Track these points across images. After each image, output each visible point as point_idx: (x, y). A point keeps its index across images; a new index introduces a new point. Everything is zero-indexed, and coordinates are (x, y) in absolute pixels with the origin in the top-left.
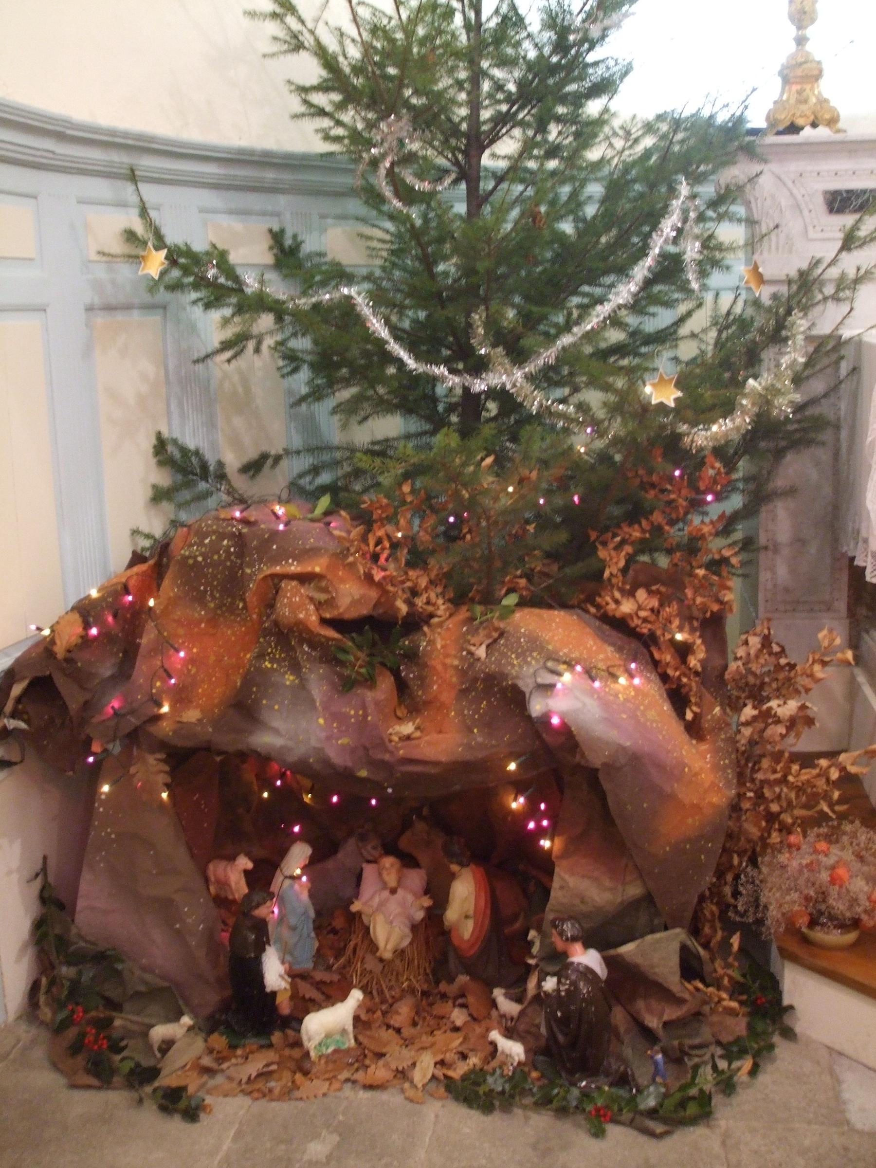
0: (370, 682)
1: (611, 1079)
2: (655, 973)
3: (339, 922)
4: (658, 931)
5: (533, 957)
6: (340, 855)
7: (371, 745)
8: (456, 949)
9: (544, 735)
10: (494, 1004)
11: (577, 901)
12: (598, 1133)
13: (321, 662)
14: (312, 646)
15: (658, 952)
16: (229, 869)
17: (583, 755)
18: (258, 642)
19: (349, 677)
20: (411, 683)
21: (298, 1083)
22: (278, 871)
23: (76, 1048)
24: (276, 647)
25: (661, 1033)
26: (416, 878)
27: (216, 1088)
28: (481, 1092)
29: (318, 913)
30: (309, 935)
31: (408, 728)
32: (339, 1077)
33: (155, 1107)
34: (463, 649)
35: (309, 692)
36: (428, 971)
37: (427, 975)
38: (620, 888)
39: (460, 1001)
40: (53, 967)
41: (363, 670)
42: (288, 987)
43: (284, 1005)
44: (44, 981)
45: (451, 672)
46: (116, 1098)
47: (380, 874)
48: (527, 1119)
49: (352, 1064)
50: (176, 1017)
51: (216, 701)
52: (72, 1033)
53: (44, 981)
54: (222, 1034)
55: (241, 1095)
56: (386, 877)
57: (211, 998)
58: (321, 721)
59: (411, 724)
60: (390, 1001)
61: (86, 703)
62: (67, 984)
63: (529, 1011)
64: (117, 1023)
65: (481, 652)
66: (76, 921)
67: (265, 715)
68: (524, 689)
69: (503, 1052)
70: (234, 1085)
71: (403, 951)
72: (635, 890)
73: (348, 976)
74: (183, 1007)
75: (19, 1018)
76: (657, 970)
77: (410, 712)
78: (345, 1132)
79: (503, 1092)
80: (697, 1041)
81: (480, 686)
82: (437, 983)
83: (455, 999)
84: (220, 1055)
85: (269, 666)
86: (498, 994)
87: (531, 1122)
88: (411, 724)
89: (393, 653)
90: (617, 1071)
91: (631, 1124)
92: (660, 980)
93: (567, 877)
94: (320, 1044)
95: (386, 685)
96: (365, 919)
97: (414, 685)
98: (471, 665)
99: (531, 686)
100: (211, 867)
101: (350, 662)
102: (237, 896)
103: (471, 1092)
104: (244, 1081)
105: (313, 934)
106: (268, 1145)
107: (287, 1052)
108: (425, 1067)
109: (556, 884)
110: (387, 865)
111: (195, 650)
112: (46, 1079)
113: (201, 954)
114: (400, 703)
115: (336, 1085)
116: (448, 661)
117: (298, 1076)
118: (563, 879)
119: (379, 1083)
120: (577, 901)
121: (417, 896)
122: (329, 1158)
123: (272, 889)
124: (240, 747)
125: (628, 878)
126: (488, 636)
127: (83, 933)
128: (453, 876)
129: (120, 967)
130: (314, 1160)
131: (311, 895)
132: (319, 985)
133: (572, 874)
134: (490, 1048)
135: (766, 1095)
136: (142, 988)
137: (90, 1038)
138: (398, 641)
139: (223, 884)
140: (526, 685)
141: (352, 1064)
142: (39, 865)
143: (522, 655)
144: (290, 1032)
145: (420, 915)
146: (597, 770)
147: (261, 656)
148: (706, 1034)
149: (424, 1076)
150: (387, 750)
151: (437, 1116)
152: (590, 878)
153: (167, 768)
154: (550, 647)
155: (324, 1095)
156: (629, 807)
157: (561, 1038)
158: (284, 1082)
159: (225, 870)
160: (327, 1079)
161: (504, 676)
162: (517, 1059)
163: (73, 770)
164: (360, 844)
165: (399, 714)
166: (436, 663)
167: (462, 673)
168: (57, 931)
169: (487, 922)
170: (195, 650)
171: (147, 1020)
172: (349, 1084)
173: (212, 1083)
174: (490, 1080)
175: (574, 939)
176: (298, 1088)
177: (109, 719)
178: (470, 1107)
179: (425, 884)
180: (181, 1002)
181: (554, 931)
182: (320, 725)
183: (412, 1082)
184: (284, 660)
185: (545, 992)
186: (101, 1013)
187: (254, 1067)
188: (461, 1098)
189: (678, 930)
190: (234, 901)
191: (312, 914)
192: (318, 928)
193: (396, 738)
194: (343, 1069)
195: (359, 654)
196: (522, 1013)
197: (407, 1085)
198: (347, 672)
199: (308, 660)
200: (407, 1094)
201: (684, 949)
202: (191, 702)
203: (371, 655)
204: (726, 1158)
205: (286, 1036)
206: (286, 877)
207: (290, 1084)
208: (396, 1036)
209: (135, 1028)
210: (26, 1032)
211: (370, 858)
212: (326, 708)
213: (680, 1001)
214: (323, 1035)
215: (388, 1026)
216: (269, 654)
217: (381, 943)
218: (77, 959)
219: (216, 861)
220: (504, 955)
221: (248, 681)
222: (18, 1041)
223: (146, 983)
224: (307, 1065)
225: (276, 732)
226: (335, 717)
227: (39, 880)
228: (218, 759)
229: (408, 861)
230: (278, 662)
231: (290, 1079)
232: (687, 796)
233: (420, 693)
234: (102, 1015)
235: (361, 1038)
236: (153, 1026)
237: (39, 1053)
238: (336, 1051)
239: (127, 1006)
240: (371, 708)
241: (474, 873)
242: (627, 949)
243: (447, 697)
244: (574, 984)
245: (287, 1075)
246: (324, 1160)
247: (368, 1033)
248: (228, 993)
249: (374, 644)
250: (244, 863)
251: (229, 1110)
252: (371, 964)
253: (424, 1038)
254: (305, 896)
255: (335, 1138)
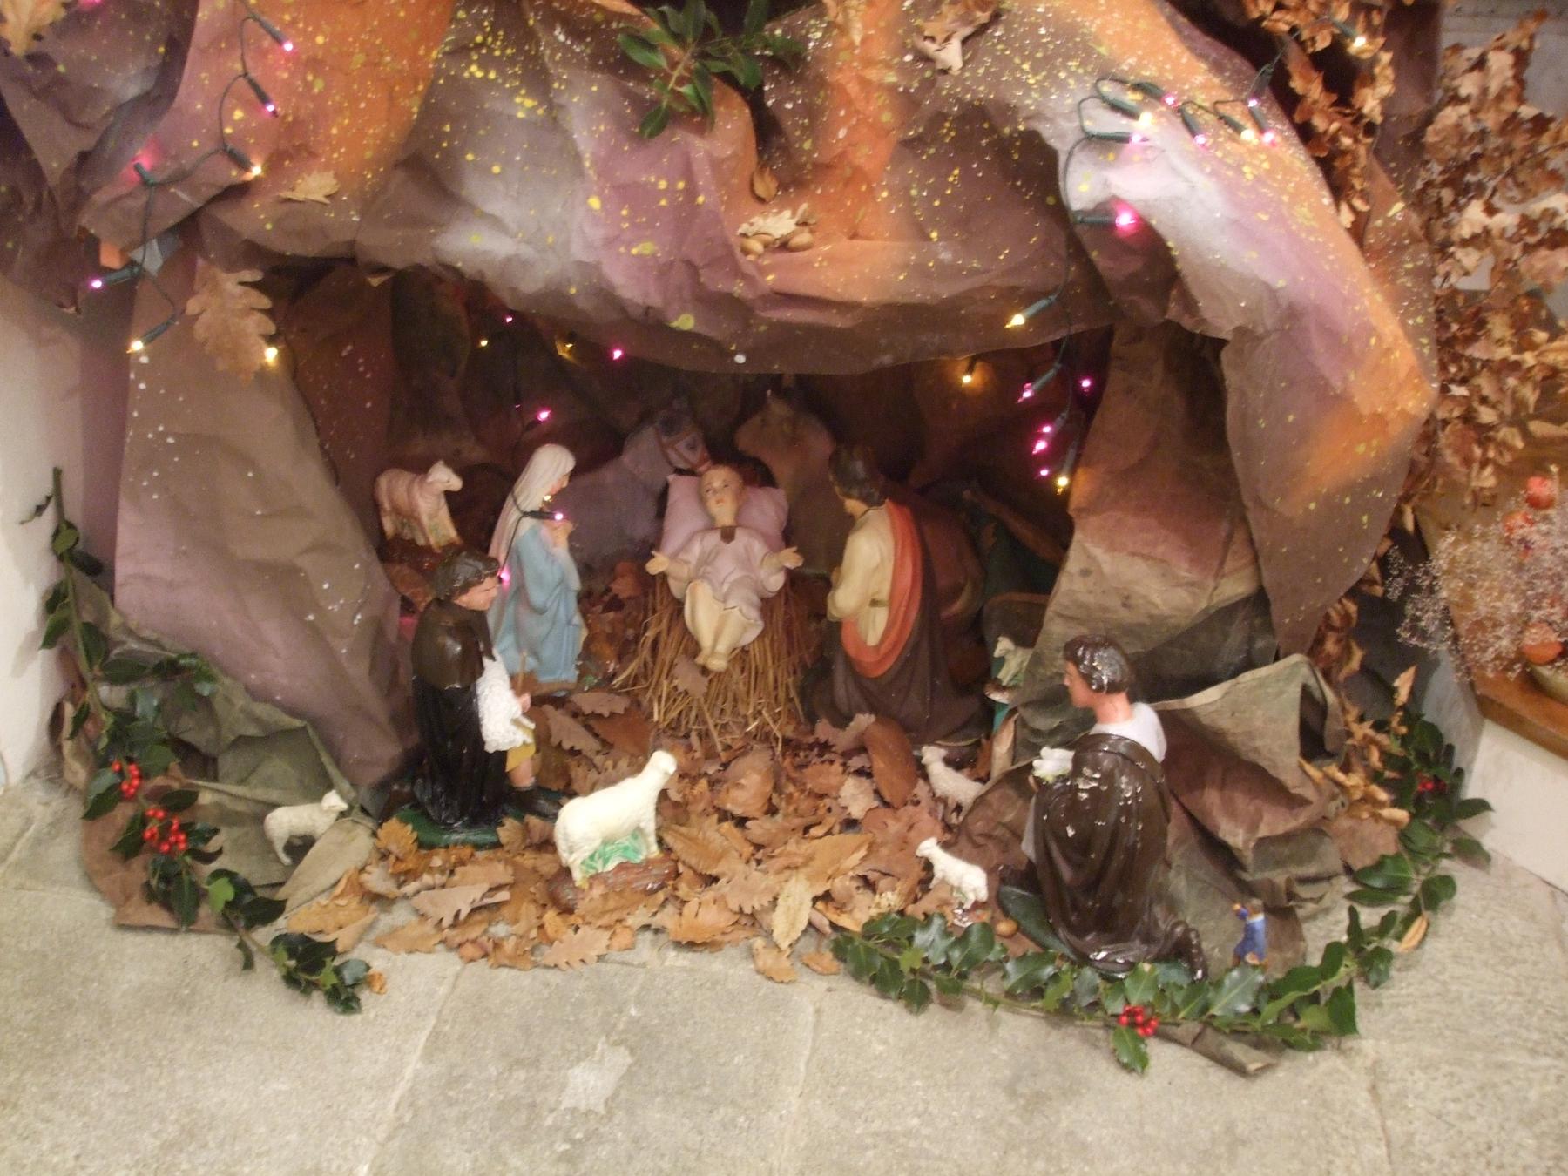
0: (700, 117)
1: (1155, 949)
2: (1256, 750)
3: (624, 587)
4: (1264, 663)
5: (1001, 688)
6: (626, 459)
7: (703, 260)
8: (849, 662)
9: (1094, 254)
10: (922, 772)
11: (1114, 602)
12: (1136, 1064)
13: (594, 67)
14: (576, 33)
15: (1258, 706)
16: (416, 487)
17: (1189, 305)
18: (454, 19)
19: (655, 102)
20: (788, 123)
21: (550, 930)
22: (509, 501)
23: (129, 846)
24: (494, 33)
25: (1249, 857)
26: (768, 508)
27: (393, 932)
28: (905, 966)
29: (586, 570)
30: (569, 623)
31: (780, 223)
32: (630, 921)
33: (276, 974)
34: (904, 50)
35: (567, 135)
36: (793, 694)
37: (791, 700)
38: (1211, 583)
39: (856, 762)
40: (84, 686)
41: (686, 90)
42: (530, 740)
43: (523, 772)
44: (69, 711)
45: (881, 99)
46: (206, 950)
47: (702, 501)
48: (993, 1024)
49: (653, 892)
50: (314, 794)
51: (369, 154)
52: (123, 814)
53: (69, 711)
54: (404, 821)
55: (440, 947)
56: (715, 508)
57: (382, 751)
58: (595, 203)
59: (787, 213)
60: (724, 756)
61: (84, 157)
62: (108, 720)
63: (994, 798)
64: (205, 798)
65: (952, 55)
66: (118, 600)
67: (471, 187)
68: (1054, 143)
69: (943, 881)
70: (429, 928)
71: (744, 651)
72: (1235, 587)
73: (645, 703)
74: (332, 770)
75: (33, 773)
76: (1258, 743)
77: (783, 186)
78: (643, 1044)
79: (947, 966)
80: (1311, 870)
81: (947, 131)
82: (812, 718)
83: (847, 755)
84: (402, 867)
85: (479, 74)
86: (933, 756)
87: (1003, 1032)
88: (787, 213)
89: (747, 52)
90: (1168, 935)
91: (1195, 1043)
92: (1264, 764)
93: (1098, 552)
94: (592, 857)
95: (733, 124)
96: (674, 585)
97: (792, 126)
98: (928, 85)
99: (1072, 137)
100: (383, 482)
101: (658, 71)
102: (432, 541)
103: (883, 961)
104: (448, 921)
105: (577, 619)
106: (493, 1071)
107: (529, 860)
108: (794, 907)
109: (1074, 562)
110: (717, 484)
111: (320, 40)
112: (71, 907)
113: (358, 671)
114: (763, 164)
115: (623, 938)
116: (872, 74)
117: (550, 916)
118: (1091, 557)
119: (707, 937)
120: (1114, 602)
121: (774, 550)
122: (611, 1101)
123: (492, 553)
124: (422, 257)
125: (1229, 565)
126: (965, 19)
127: (133, 625)
128: (848, 525)
129: (205, 689)
130: (583, 1108)
131: (572, 550)
132: (589, 721)
133: (1112, 547)
134: (917, 872)
135: (1444, 983)
136: (252, 731)
137: (153, 827)
138: (760, 28)
139: (408, 516)
140: (1059, 134)
141: (653, 892)
142: (47, 487)
143: (1046, 64)
144: (533, 821)
145: (776, 582)
146: (1221, 343)
147: (461, 51)
148: (1330, 856)
149: (793, 925)
150: (738, 273)
151: (818, 1012)
152: (1147, 558)
153: (266, 303)
154: (1103, 50)
155: (600, 958)
156: (1262, 423)
157: (1066, 872)
158: (520, 928)
159: (409, 491)
160: (607, 927)
161: (1008, 111)
162: (972, 898)
163: (74, 302)
164: (665, 439)
165: (760, 190)
166: (845, 77)
167: (908, 103)
168: (87, 617)
169: (914, 614)
170: (320, 40)
171: (261, 794)
172: (648, 935)
173: (387, 921)
174: (920, 938)
175: (1113, 688)
176: (551, 943)
177: (130, 195)
178: (884, 995)
179: (783, 517)
180: (325, 759)
181: (1071, 668)
182: (590, 210)
183: (769, 934)
184: (512, 61)
185: (1038, 780)
186: (174, 779)
187: (464, 896)
188: (867, 979)
189: (1296, 658)
190: (427, 550)
191: (575, 583)
192: (586, 600)
193: (756, 246)
194: (635, 904)
195: (675, 51)
196: (980, 801)
197: (759, 943)
198: (649, 93)
199: (565, 62)
200: (760, 963)
201: (1306, 692)
202: (313, 155)
203: (703, 56)
204: (1384, 1128)
205: (526, 829)
206: (525, 514)
207: (534, 933)
208: (736, 832)
209: (240, 807)
210: (43, 805)
211: (682, 465)
212: (604, 171)
213: (1293, 802)
214: (598, 842)
215: (724, 816)
216: (479, 46)
217: (706, 640)
218: (126, 671)
219: (396, 471)
220: (945, 681)
221: (432, 111)
222: (29, 821)
223: (257, 720)
224: (567, 895)
225: (496, 223)
226: (628, 194)
227: (50, 513)
228: (375, 281)
229: (756, 474)
230: (498, 64)
231: (535, 921)
232: (1367, 396)
233: (807, 145)
234: (176, 786)
235: (669, 839)
236: (274, 806)
237: (65, 850)
238: (622, 867)
239: (226, 763)
240: (704, 177)
241: (890, 514)
242: (1203, 701)
243: (866, 156)
244: (1108, 778)
245: (529, 911)
246: (602, 1110)
247: (683, 830)
248: (415, 739)
249: (707, 33)
250: (444, 478)
251: (416, 981)
252: (686, 678)
253: (792, 847)
254: (562, 551)
255: (622, 1058)
